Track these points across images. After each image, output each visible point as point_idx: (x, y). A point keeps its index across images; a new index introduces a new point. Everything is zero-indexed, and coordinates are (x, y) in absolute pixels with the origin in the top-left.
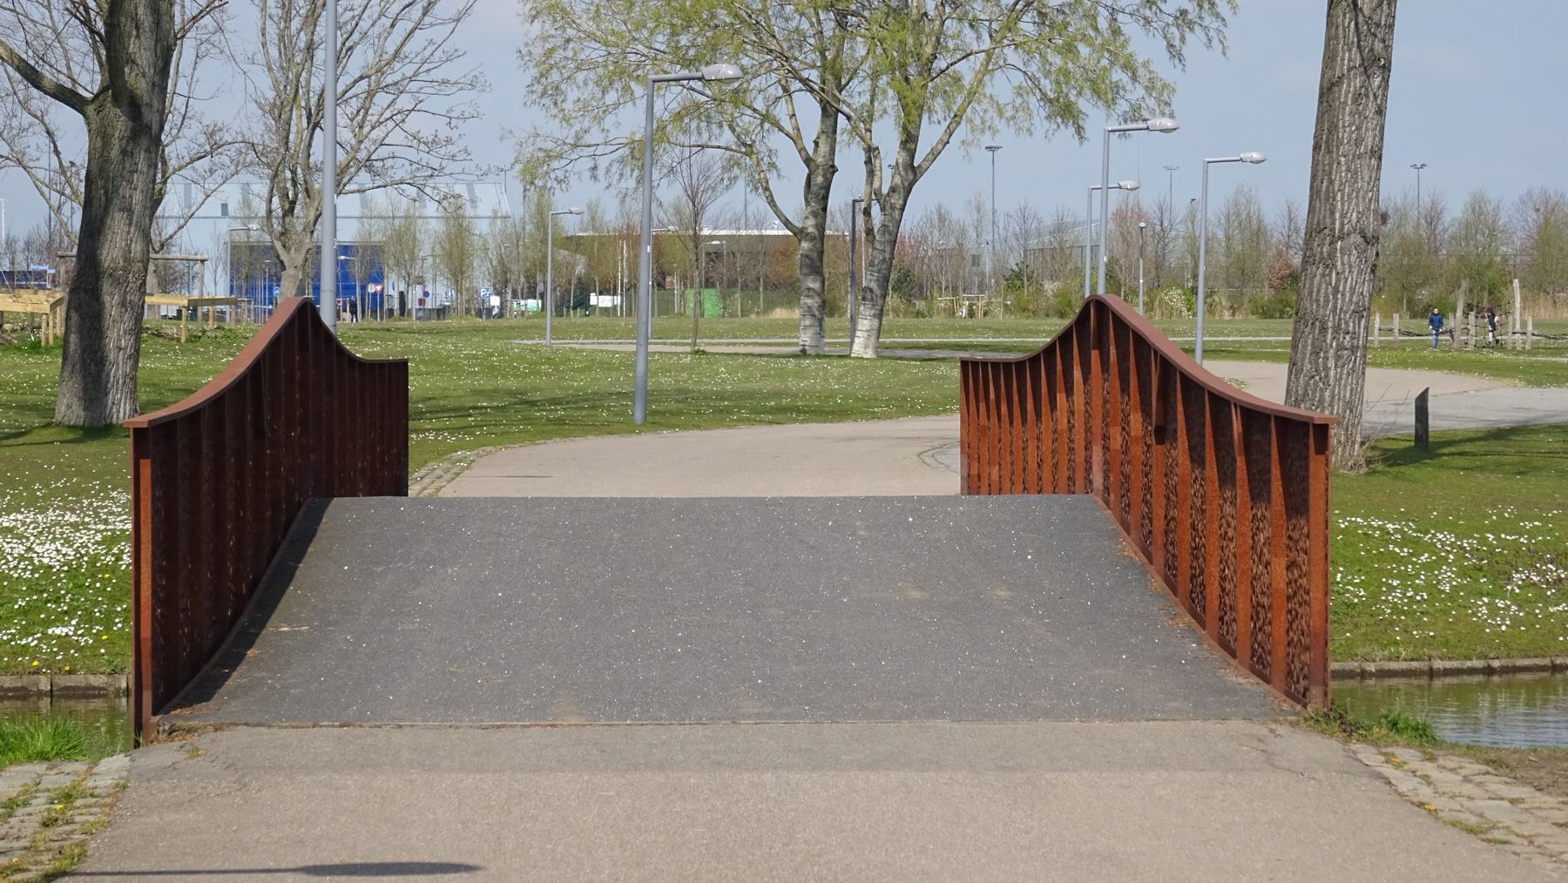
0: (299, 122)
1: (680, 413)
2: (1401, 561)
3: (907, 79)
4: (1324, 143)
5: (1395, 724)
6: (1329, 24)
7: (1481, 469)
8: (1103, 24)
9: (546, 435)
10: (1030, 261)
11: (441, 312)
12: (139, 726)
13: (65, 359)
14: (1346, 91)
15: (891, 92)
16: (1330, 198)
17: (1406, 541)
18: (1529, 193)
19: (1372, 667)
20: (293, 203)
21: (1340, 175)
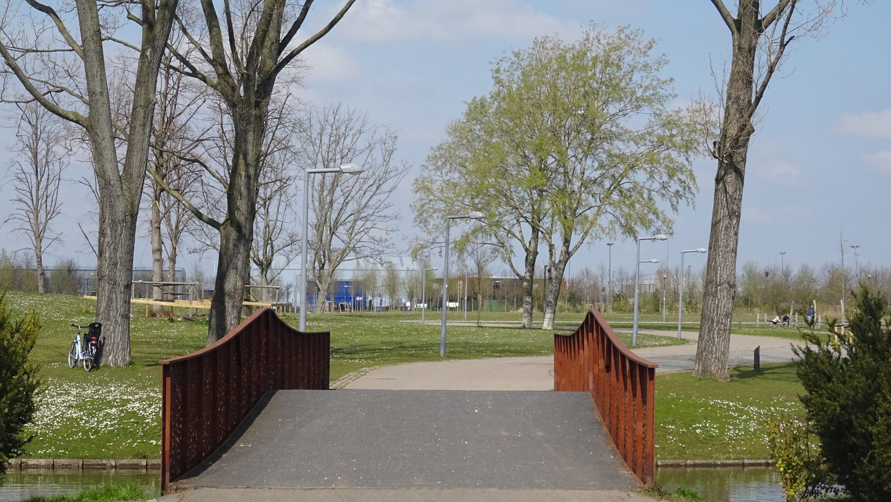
0: (326, 232)
1: (461, 352)
2: (735, 418)
3: (566, 218)
4: (713, 246)
5: (683, 492)
6: (715, 198)
7: (779, 379)
8: (645, 196)
9: (403, 361)
10: (624, 291)
11: (387, 308)
12: (164, 487)
13: (210, 328)
14: (722, 226)
15: (558, 223)
16: (715, 269)
17: (737, 410)
18: (826, 265)
19: (719, 462)
20: (324, 265)
21: (719, 260)
